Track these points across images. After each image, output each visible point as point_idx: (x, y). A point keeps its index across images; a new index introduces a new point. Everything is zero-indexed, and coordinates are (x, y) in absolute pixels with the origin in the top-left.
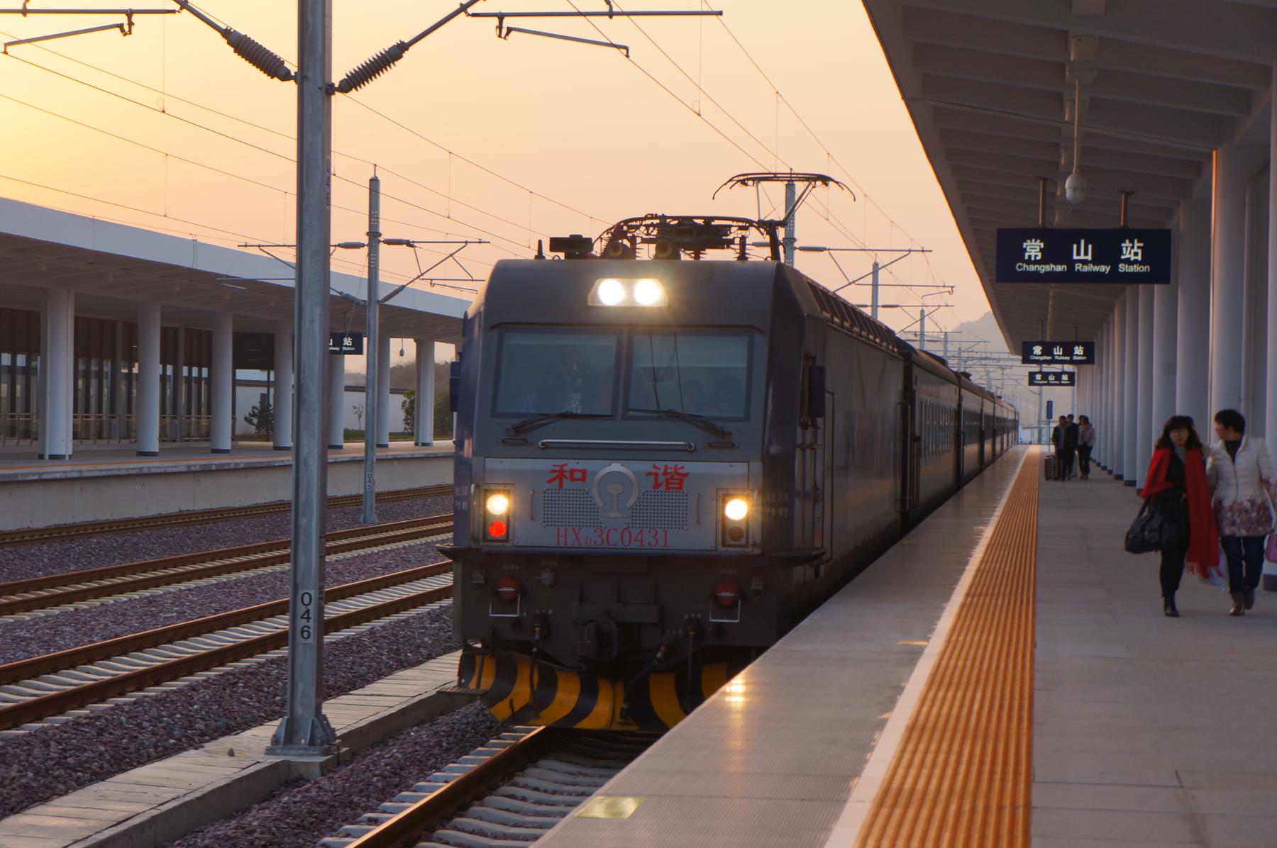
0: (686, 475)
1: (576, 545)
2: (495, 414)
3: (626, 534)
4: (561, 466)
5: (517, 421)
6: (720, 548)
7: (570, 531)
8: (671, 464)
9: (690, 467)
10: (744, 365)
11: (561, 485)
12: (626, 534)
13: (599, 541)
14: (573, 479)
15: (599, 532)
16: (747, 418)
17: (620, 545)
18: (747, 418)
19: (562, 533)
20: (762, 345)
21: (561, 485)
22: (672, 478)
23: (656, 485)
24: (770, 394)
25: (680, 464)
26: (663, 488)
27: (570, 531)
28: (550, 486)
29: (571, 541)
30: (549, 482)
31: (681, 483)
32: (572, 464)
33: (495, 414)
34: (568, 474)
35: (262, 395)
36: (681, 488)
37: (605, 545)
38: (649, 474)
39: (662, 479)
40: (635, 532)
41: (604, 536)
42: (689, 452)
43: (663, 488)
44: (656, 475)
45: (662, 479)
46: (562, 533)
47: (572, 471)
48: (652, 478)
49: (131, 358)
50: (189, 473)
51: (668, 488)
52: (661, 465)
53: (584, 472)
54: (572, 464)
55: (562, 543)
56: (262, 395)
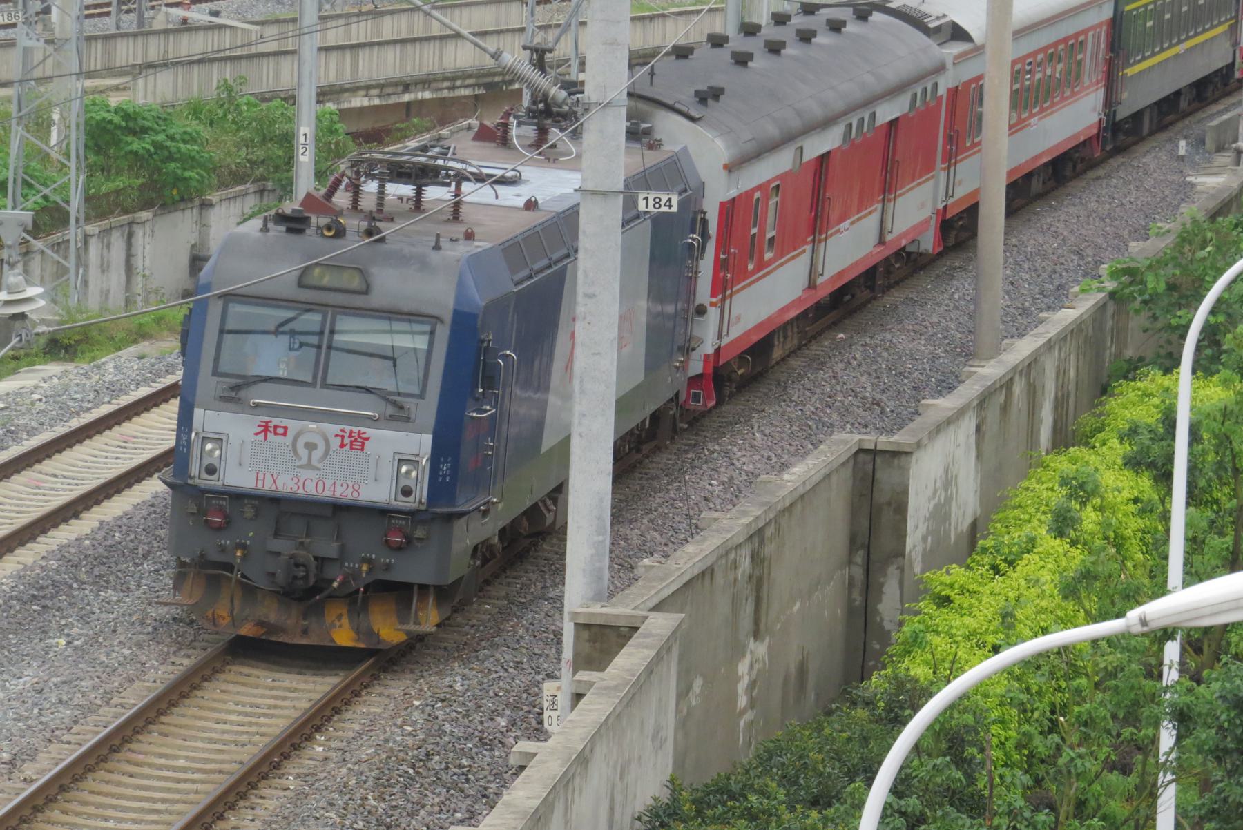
0: (367, 439)
1: (274, 488)
2: (215, 373)
3: (320, 484)
5: (234, 381)
6: (393, 502)
7: (268, 477)
8: (356, 429)
9: (369, 432)
11: (266, 438)
12: (320, 484)
13: (295, 488)
14: (276, 434)
16: (421, 396)
18: (421, 396)
19: (261, 477)
20: (443, 333)
21: (266, 438)
23: (342, 446)
25: (363, 430)
26: (348, 448)
27: (268, 477)
32: (276, 421)
33: (215, 373)
35: (583, 71)
36: (362, 449)
37: (301, 491)
39: (347, 440)
40: (329, 483)
41: (301, 484)
42: (373, 421)
43: (348, 448)
44: (343, 437)
45: (347, 440)
46: (261, 477)
47: (276, 427)
48: (339, 439)
49: (1167, 371)
50: (407, 87)
52: (348, 428)
53: (286, 428)
54: (276, 421)
55: (260, 486)
56: (583, 71)
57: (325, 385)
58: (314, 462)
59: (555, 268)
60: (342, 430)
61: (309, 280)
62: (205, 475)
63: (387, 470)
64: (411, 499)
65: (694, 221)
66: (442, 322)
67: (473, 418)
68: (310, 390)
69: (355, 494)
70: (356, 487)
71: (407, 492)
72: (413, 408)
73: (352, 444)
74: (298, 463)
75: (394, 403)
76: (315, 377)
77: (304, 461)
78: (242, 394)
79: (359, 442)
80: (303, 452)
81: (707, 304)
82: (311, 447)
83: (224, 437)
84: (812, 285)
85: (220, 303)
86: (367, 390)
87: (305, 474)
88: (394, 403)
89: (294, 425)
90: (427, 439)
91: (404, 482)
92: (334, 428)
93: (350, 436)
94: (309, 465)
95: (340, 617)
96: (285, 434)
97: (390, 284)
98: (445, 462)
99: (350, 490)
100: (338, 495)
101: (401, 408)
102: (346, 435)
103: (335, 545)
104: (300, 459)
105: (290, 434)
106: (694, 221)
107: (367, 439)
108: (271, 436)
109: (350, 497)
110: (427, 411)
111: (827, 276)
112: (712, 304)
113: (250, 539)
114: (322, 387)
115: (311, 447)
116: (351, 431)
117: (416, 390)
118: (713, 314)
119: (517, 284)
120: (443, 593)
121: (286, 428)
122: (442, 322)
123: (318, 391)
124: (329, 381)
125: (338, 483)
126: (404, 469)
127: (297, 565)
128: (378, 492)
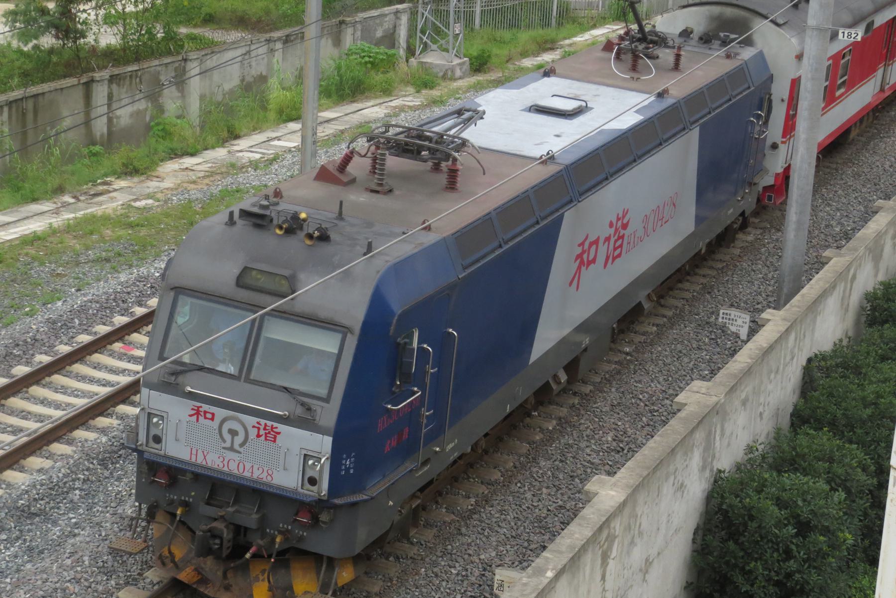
0: (279, 433)
3: (241, 466)
4: (199, 407)
6: (300, 489)
7: (200, 452)
9: (281, 428)
10: (336, 351)
11: (197, 420)
12: (241, 466)
13: (221, 465)
14: (206, 418)
15: (222, 459)
16: (327, 400)
17: (236, 471)
18: (327, 400)
19: (194, 452)
20: (352, 343)
21: (197, 420)
22: (269, 433)
23: (259, 436)
24: (725, 106)
25: (275, 424)
28: (190, 418)
29: (200, 460)
30: (191, 416)
31: (275, 438)
32: (205, 407)
34: (202, 414)
36: (274, 441)
37: (226, 469)
38: (254, 427)
39: (262, 432)
41: (226, 463)
43: (263, 438)
44: (259, 428)
45: (262, 432)
46: (194, 452)
47: (205, 412)
48: (256, 430)
51: (266, 439)
55: (193, 460)
57: (248, 380)
58: (236, 447)
59: (542, 224)
60: (258, 423)
61: (248, 281)
62: (152, 444)
63: (296, 463)
64: (315, 488)
65: (761, 101)
66: (352, 333)
67: (388, 409)
68: (236, 382)
69: (269, 478)
70: (270, 472)
71: (313, 481)
72: (319, 410)
73: (266, 436)
74: (224, 445)
75: (303, 404)
76: (241, 370)
77: (228, 444)
78: (181, 379)
79: (272, 436)
80: (227, 437)
81: (779, 142)
82: (233, 433)
83: (164, 415)
84: (882, 90)
85: (172, 294)
86: (286, 389)
87: (230, 455)
88: (303, 404)
89: (221, 413)
90: (328, 441)
91: (310, 473)
92: (250, 420)
93: (265, 429)
94: (231, 449)
95: (263, 572)
96: (212, 419)
97: (312, 289)
98: (349, 457)
99: (265, 474)
100: (255, 476)
101: (309, 409)
102: (262, 427)
103: (255, 516)
104: (224, 441)
105: (217, 420)
106: (761, 101)
107: (279, 433)
108: (201, 419)
109: (265, 480)
110: (329, 414)
111: (892, 82)
112: (783, 142)
113: (193, 497)
114: (245, 381)
115: (233, 433)
116: (266, 425)
117: (323, 392)
118: (783, 148)
119: (465, 268)
120: (357, 559)
121: (213, 414)
122: (352, 333)
123: (242, 386)
124: (252, 377)
125: (256, 467)
126: (310, 462)
127: (214, 536)
128: (287, 478)
